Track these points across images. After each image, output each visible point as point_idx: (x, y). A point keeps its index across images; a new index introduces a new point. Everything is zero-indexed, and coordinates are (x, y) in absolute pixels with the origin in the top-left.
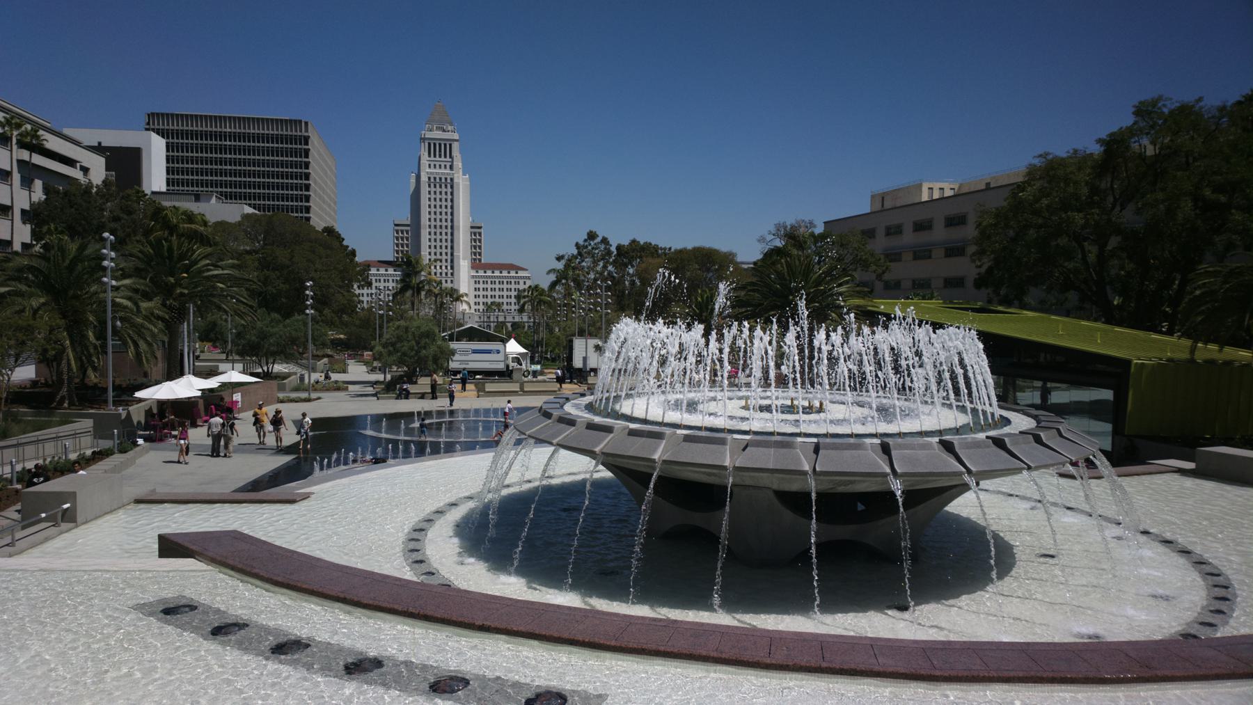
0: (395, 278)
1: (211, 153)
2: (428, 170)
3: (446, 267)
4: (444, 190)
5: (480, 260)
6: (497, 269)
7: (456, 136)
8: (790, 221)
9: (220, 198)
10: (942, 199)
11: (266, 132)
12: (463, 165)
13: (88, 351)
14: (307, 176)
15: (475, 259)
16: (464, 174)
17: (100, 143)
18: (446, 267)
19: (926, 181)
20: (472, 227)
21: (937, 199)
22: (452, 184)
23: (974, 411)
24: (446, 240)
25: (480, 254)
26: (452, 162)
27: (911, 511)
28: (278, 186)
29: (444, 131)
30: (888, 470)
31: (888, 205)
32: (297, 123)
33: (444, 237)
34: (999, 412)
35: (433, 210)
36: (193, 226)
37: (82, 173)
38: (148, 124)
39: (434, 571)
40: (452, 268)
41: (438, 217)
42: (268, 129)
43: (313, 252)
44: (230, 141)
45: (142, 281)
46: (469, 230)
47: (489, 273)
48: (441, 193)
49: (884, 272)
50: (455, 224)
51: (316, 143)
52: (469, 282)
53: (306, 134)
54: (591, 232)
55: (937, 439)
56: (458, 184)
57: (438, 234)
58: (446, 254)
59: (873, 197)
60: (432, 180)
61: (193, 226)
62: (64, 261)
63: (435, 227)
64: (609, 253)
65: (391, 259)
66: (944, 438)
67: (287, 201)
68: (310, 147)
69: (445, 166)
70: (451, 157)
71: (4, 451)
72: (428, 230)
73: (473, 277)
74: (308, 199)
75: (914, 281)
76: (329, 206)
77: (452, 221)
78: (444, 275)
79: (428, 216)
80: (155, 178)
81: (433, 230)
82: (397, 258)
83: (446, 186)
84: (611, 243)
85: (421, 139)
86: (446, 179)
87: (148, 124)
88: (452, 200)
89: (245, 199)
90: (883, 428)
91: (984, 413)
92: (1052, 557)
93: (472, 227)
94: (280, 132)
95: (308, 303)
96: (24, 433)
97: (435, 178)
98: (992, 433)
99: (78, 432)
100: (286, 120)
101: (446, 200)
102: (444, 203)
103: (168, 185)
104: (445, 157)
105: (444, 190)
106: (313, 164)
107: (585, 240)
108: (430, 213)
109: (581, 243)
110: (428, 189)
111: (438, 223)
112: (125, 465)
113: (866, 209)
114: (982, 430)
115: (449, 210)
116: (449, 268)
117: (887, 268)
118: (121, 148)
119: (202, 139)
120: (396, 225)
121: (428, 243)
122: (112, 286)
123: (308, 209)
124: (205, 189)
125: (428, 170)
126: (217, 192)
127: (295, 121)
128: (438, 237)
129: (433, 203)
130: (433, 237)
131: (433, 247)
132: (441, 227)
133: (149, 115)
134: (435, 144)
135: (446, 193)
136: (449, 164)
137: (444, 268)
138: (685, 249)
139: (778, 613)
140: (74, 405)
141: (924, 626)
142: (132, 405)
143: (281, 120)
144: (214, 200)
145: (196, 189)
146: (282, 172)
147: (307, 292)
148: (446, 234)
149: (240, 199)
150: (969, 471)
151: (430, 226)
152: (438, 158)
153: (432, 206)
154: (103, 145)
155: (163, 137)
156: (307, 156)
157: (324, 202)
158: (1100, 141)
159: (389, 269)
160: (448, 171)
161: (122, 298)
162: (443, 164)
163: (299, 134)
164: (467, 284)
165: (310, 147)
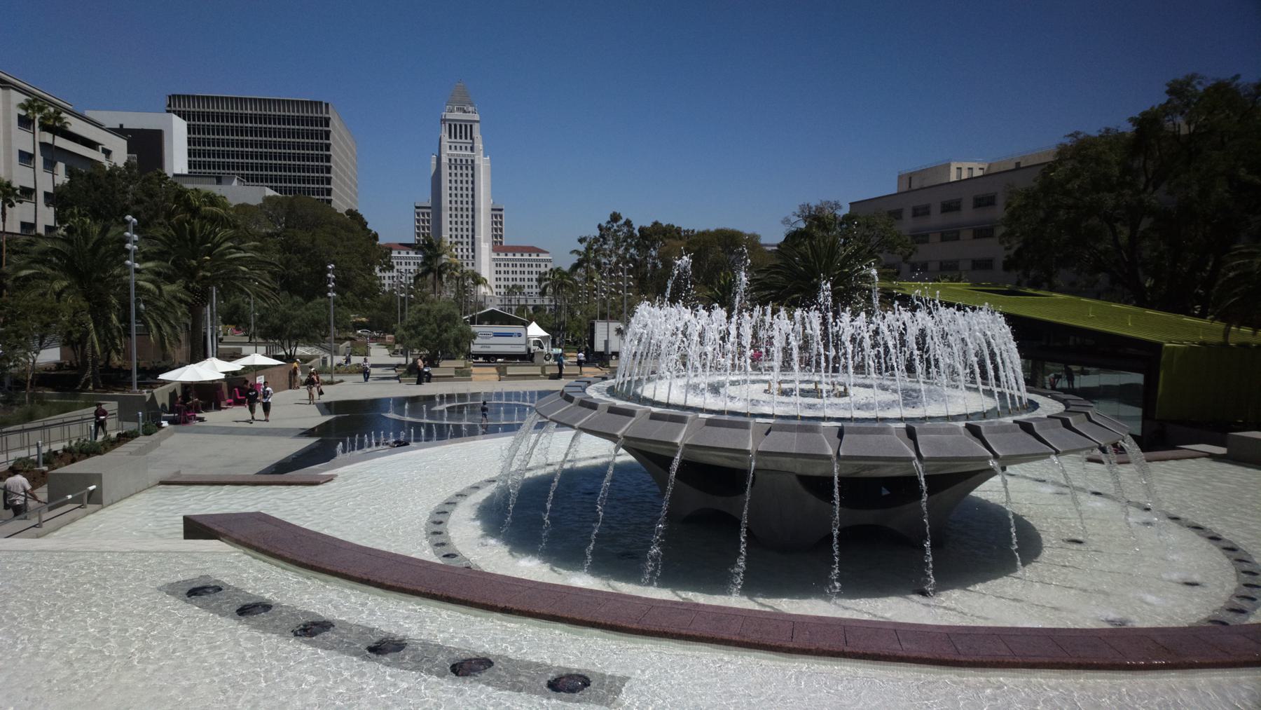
0: (416, 261)
2: (449, 152)
5: (501, 243)
7: (477, 117)
12: (484, 147)
13: (112, 334)
14: (328, 158)
15: (496, 242)
16: (485, 156)
17: (121, 126)
19: (955, 161)
20: (493, 210)
23: (1002, 395)
24: (467, 223)
25: (501, 236)
26: (473, 143)
29: (465, 112)
30: (913, 455)
31: (915, 185)
32: (317, 104)
33: (465, 219)
35: (454, 192)
37: (104, 155)
38: (170, 106)
40: (473, 250)
41: (459, 199)
46: (490, 213)
47: (510, 256)
49: (911, 254)
50: (476, 206)
53: (327, 116)
54: (615, 213)
55: (962, 424)
57: (459, 216)
58: (467, 236)
59: (900, 177)
60: (453, 162)
61: (214, 209)
62: (87, 244)
63: (456, 209)
64: (631, 235)
65: (412, 241)
70: (471, 138)
72: (449, 212)
73: (494, 260)
74: (329, 181)
76: (350, 188)
77: (473, 203)
80: (177, 160)
81: (454, 213)
82: (419, 241)
83: (467, 168)
85: (442, 120)
87: (170, 106)
89: (267, 182)
93: (493, 210)
97: (456, 160)
99: (85, 417)
103: (190, 167)
104: (466, 138)
105: (465, 171)
106: (334, 147)
107: (608, 222)
108: (451, 195)
109: (604, 224)
110: (449, 171)
111: (459, 206)
112: (149, 448)
113: (893, 189)
114: (1010, 413)
116: (470, 250)
118: (142, 130)
120: (417, 208)
125: (449, 152)
126: (238, 174)
127: (316, 103)
128: (459, 219)
129: (454, 185)
130: (454, 219)
132: (462, 209)
133: (170, 97)
135: (467, 175)
136: (470, 145)
137: (465, 250)
138: (708, 231)
140: (99, 388)
144: (235, 182)
145: (218, 171)
147: (329, 275)
148: (467, 216)
151: (451, 209)
152: (458, 140)
153: (453, 189)
155: (184, 119)
156: (328, 138)
158: (1131, 120)
160: (469, 152)
161: (145, 280)
162: (463, 146)
163: (320, 115)
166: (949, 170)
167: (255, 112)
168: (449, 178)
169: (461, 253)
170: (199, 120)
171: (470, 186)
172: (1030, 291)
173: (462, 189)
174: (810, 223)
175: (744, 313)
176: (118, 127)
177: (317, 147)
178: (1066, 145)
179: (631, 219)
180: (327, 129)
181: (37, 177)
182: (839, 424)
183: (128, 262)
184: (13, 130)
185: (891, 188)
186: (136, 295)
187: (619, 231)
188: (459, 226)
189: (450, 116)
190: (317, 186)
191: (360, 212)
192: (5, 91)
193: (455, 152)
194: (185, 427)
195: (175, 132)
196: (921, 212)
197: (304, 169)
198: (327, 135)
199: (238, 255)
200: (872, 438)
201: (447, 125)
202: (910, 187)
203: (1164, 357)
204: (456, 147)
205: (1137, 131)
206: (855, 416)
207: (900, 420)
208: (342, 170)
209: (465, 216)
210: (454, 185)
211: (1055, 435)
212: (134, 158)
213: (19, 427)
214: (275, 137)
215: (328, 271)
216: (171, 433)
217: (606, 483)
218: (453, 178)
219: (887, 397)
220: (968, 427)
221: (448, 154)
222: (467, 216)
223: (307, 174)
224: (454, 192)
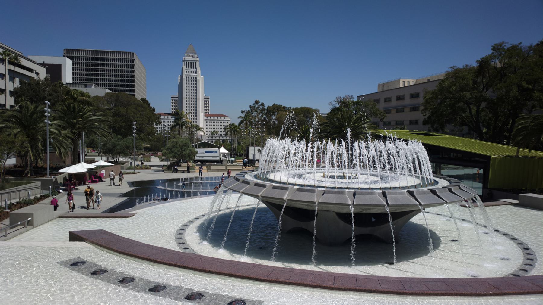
2: (186, 74)
3: (194, 116)
4: (193, 82)
5: (208, 113)
6: (216, 117)
7: (198, 59)
12: (201, 72)
14: (134, 76)
16: (201, 76)
17: (44, 62)
18: (194, 116)
20: (205, 99)
23: (423, 178)
24: (194, 104)
26: (196, 70)
29: (193, 57)
31: (385, 89)
33: (193, 103)
34: (433, 178)
36: (84, 98)
38: (65, 54)
40: (196, 116)
41: (190, 94)
43: (136, 109)
46: (204, 100)
48: (191, 84)
49: (384, 118)
50: (198, 97)
51: (137, 61)
52: (204, 122)
53: (133, 58)
55: (406, 190)
57: (190, 101)
59: (379, 85)
60: (188, 78)
61: (84, 98)
63: (189, 98)
64: (264, 110)
65: (170, 112)
67: (125, 87)
69: (193, 72)
70: (196, 68)
72: (186, 100)
74: (134, 86)
76: (143, 89)
77: (196, 96)
80: (68, 77)
81: (188, 100)
82: (173, 112)
83: (194, 81)
84: (265, 105)
85: (183, 60)
86: (194, 78)
87: (65, 54)
88: (196, 87)
89: (107, 86)
91: (427, 179)
93: (205, 99)
96: (11, 188)
97: (189, 77)
98: (431, 188)
99: (34, 187)
102: (193, 88)
103: (73, 80)
104: (193, 68)
105: (193, 82)
106: (136, 71)
107: (254, 104)
108: (187, 92)
109: (252, 105)
110: (186, 82)
111: (190, 97)
115: (195, 91)
116: (195, 116)
121: (186, 105)
122: (49, 124)
125: (186, 74)
126: (94, 83)
127: (128, 53)
128: (190, 103)
129: (188, 88)
131: (188, 107)
133: (65, 50)
135: (194, 84)
136: (195, 71)
137: (193, 116)
144: (93, 87)
145: (85, 82)
147: (134, 127)
148: (194, 101)
149: (105, 86)
150: (420, 204)
151: (187, 98)
152: (190, 69)
154: (45, 63)
155: (71, 59)
156: (133, 68)
158: (477, 61)
160: (195, 74)
163: (130, 58)
164: (203, 123)
166: (399, 82)
168: (186, 85)
171: (195, 88)
176: (42, 63)
177: (129, 72)
179: (263, 102)
182: (353, 191)
183: (46, 121)
185: (374, 89)
189: (186, 59)
193: (189, 74)
195: (67, 65)
198: (133, 66)
201: (185, 63)
202: (383, 89)
204: (191, 72)
207: (380, 189)
211: (445, 195)
217: (232, 216)
218: (188, 85)
220: (408, 191)
221: (186, 75)
222: (194, 101)
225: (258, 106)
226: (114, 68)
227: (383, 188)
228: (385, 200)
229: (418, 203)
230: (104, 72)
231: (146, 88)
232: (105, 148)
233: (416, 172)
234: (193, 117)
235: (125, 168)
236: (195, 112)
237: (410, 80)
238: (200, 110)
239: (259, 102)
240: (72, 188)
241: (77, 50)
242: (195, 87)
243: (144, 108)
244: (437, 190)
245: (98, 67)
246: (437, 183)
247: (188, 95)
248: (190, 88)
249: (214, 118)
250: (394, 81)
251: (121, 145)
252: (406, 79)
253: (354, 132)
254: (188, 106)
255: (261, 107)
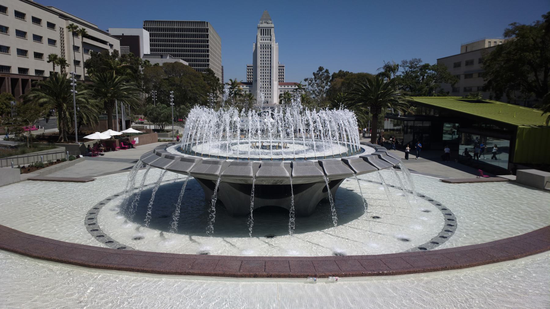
0: (292, 90)
1: (158, 37)
2: (260, 41)
3: (268, 85)
4: (267, 50)
5: (283, 81)
6: (290, 85)
7: (273, 25)
8: (409, 59)
9: (171, 57)
10: (490, 48)
11: (180, 27)
14: (208, 46)
15: (281, 81)
16: (276, 43)
17: (123, 34)
18: (268, 85)
19: (487, 38)
20: (279, 67)
21: (487, 48)
22: (270, 47)
23: (348, 145)
25: (283, 79)
26: (271, 37)
27: (296, 195)
28: (194, 51)
29: (268, 23)
30: (323, 174)
31: (469, 50)
32: (203, 23)
33: (267, 71)
34: (360, 146)
37: (110, 47)
38: (144, 25)
39: (451, 213)
40: (270, 85)
41: (265, 62)
42: (190, 26)
44: (177, 32)
45: (91, 91)
46: (278, 68)
48: (266, 51)
49: (455, 83)
50: (272, 65)
52: (278, 91)
53: (207, 28)
55: (340, 159)
56: (273, 47)
58: (268, 79)
59: (462, 46)
60: (262, 46)
62: (58, 83)
63: (263, 67)
64: (328, 77)
66: (342, 158)
67: (200, 57)
68: (209, 33)
70: (270, 35)
71: (2, 160)
72: (260, 68)
74: (208, 56)
75: (478, 87)
76: (218, 59)
77: (270, 64)
78: (267, 88)
79: (260, 62)
80: (145, 48)
81: (262, 68)
82: (248, 81)
83: (268, 48)
84: (330, 72)
85: (258, 27)
86: (268, 45)
88: (271, 55)
90: (318, 154)
91: (356, 146)
92: (378, 218)
94: (197, 27)
95: (171, 100)
96: (34, 152)
97: (263, 45)
99: (57, 152)
100: (199, 22)
101: (268, 55)
102: (267, 56)
105: (267, 50)
106: (210, 41)
107: (318, 71)
108: (261, 61)
109: (316, 72)
110: (260, 50)
111: (265, 65)
112: (69, 166)
113: (458, 52)
115: (269, 59)
116: (269, 85)
117: (456, 81)
118: (131, 36)
119: (175, 32)
120: (248, 67)
121: (260, 74)
122: (76, 93)
123: (208, 61)
124: (164, 53)
127: (203, 22)
128: (265, 71)
129: (262, 56)
130: (262, 71)
131: (262, 76)
132: (263, 67)
133: (144, 22)
134: (263, 30)
135: (268, 52)
136: (269, 39)
137: (267, 85)
139: (239, 237)
141: (327, 248)
142: (86, 142)
143: (184, 22)
145: (162, 53)
146: (183, 44)
147: (171, 96)
148: (268, 70)
149: (176, 57)
151: (261, 67)
152: (265, 36)
154: (124, 35)
155: (148, 31)
156: (207, 37)
157: (216, 57)
159: (244, 86)
160: (269, 42)
162: (267, 39)
163: (204, 27)
164: (276, 92)
165: (209, 33)
166: (485, 43)
167: (169, 27)
168: (260, 53)
169: (265, 86)
170: (164, 31)
172: (488, 101)
173: (266, 58)
174: (386, 69)
175: (307, 112)
176: (122, 35)
178: (509, 29)
179: (328, 69)
180: (207, 33)
181: (75, 56)
182: (290, 162)
184: (70, 37)
185: (457, 51)
186: (76, 104)
187: (323, 75)
188: (265, 74)
189: (261, 26)
190: (203, 58)
191: (345, 70)
192: (67, 21)
194: (94, 158)
195: (144, 36)
196: (469, 63)
197: (198, 51)
198: (207, 36)
199: (124, 88)
200: (240, 167)
201: (260, 30)
203: (518, 132)
204: (263, 39)
205: (546, 21)
206: (306, 157)
207: (315, 158)
208: (214, 50)
209: (267, 70)
210: (262, 56)
212: (128, 48)
213: (16, 156)
214: (196, 38)
215: (171, 94)
216: (83, 160)
218: (262, 53)
219: (301, 148)
220: (342, 160)
221: (260, 43)
223: (186, 53)
224: (262, 59)
225: (322, 73)
226: (178, 38)
227: (319, 158)
228: (322, 170)
229: (353, 172)
230: (186, 42)
231: (221, 58)
232: (151, 116)
233: (341, 139)
234: (265, 86)
235: (169, 136)
236: (269, 80)
237: (498, 40)
238: (274, 79)
239: (324, 69)
240: (96, 153)
241: (156, 21)
242: (269, 55)
243: (198, 77)
244: (368, 157)
245: (175, 37)
246: (363, 150)
247: (262, 64)
248: (265, 56)
249: (288, 87)
250: (478, 42)
251: (164, 114)
252: (493, 38)
253: (381, 99)
254: (262, 74)
255: (326, 74)
